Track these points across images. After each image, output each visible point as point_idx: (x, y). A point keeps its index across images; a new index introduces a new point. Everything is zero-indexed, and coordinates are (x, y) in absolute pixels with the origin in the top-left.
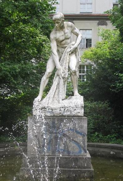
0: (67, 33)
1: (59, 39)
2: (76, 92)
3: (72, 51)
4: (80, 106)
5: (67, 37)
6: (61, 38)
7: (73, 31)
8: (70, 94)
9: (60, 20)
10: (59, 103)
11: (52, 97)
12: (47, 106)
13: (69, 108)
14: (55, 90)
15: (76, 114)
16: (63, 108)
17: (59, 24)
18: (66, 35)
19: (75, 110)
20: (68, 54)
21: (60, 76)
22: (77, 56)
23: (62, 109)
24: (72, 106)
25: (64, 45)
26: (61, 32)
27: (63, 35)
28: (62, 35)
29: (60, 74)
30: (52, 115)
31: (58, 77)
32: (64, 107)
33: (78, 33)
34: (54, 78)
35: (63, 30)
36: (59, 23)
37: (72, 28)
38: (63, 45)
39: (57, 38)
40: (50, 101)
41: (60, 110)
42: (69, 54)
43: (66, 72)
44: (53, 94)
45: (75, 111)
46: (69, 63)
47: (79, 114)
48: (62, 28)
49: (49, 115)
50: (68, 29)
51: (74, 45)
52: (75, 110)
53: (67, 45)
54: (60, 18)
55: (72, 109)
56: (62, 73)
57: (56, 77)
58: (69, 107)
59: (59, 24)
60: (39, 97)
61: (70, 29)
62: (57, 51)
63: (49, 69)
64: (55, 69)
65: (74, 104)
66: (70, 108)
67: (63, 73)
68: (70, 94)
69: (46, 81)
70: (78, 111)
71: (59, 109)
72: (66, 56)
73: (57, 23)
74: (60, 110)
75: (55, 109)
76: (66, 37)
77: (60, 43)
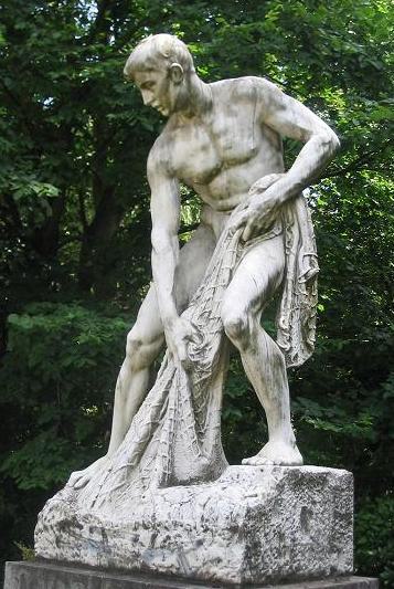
0: (225, 132)
1: (188, 170)
3: (251, 221)
4: (222, 523)
5: (229, 154)
6: (200, 164)
7: (271, 121)
8: (242, 435)
9: (150, 70)
12: (83, 512)
13: (172, 534)
15: (204, 570)
16: (146, 528)
17: (157, 88)
18: (222, 142)
19: (200, 543)
22: (293, 250)
23: (145, 535)
24: (186, 521)
25: (229, 195)
26: (194, 130)
27: (204, 148)
28: (200, 144)
30: (104, 561)
32: (153, 526)
33: (301, 124)
35: (201, 123)
36: (153, 83)
37: (259, 106)
38: (221, 198)
39: (175, 164)
41: (135, 540)
42: (241, 241)
43: (208, 338)
45: (201, 552)
47: (219, 572)
49: (93, 562)
50: (230, 113)
52: (200, 543)
55: (185, 538)
58: (175, 524)
59: (157, 88)
61: (246, 112)
65: (199, 511)
66: (180, 530)
67: (188, 339)
70: (215, 550)
71: (130, 535)
74: (135, 540)
75: (116, 534)
76: (222, 154)
77: (196, 191)
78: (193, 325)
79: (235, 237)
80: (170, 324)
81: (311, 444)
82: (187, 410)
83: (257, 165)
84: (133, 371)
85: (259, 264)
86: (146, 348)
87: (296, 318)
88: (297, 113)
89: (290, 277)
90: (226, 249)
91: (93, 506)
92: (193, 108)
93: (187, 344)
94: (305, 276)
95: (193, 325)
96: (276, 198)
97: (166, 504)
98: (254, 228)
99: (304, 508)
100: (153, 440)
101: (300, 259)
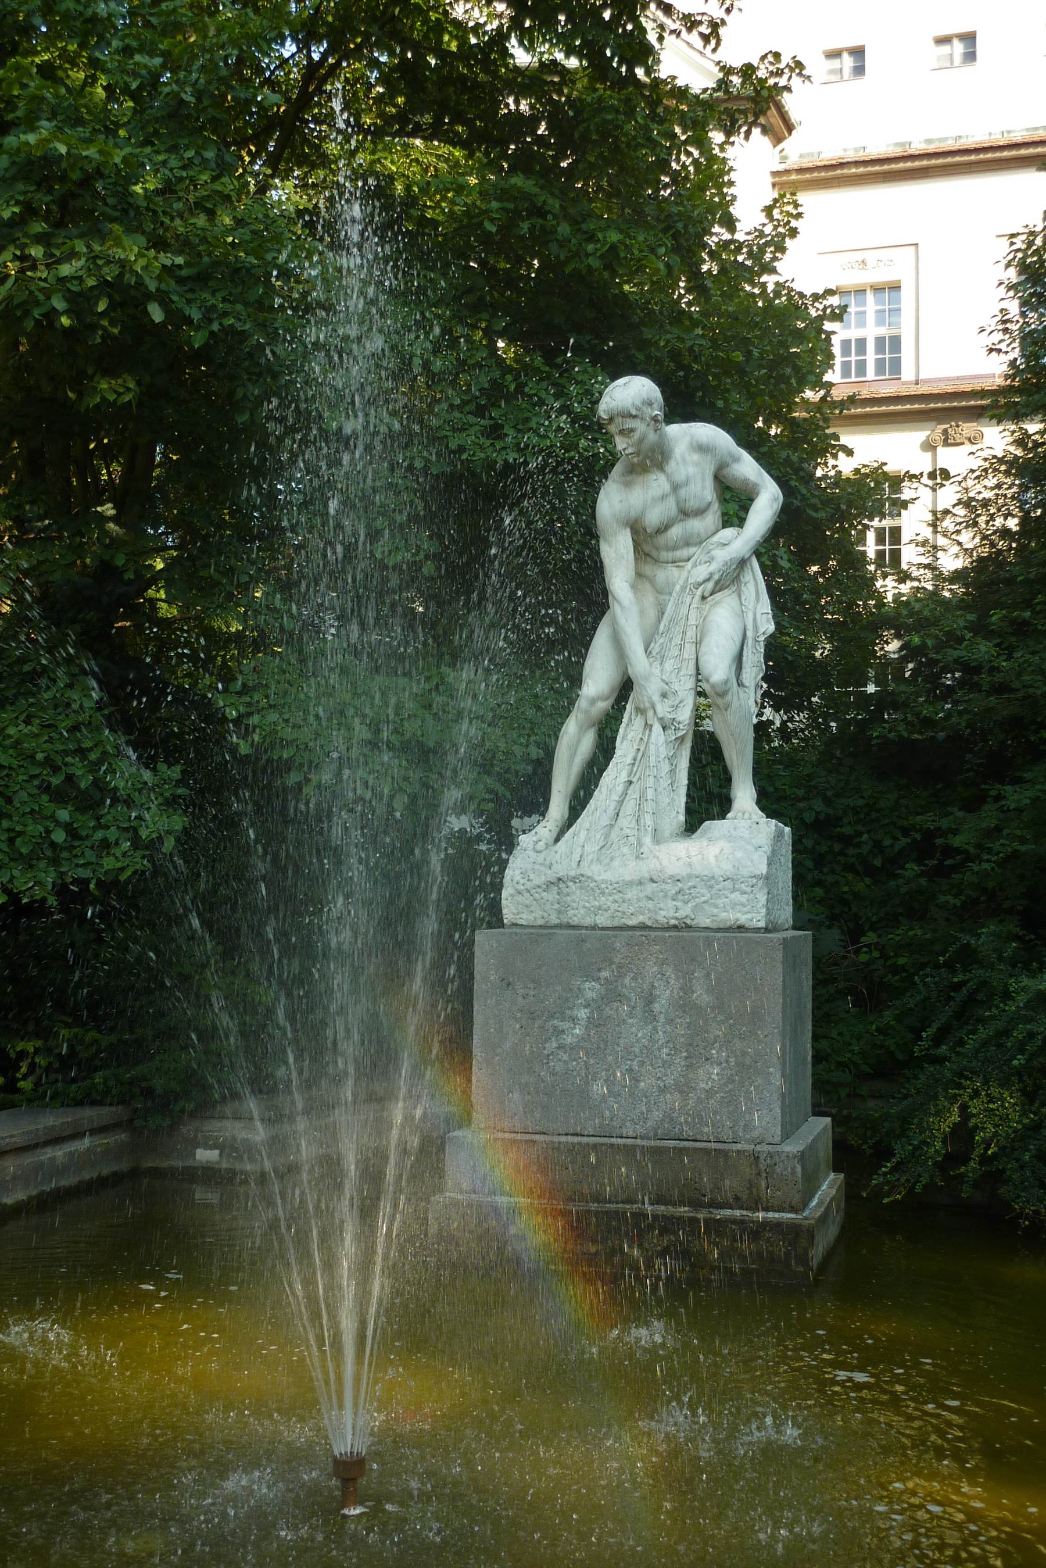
2: (744, 794)
3: (716, 577)
5: (693, 504)
7: (725, 471)
8: (707, 801)
9: (635, 417)
10: (637, 857)
14: (620, 789)
18: (683, 492)
20: (697, 598)
21: (650, 713)
27: (664, 497)
29: (647, 705)
31: (638, 722)
36: (632, 430)
40: (592, 848)
42: (703, 598)
44: (611, 811)
46: (698, 643)
48: (654, 459)
53: (692, 550)
56: (656, 698)
57: (630, 719)
60: (546, 828)
62: (758, 802)
63: (597, 679)
64: (625, 688)
67: (664, 695)
68: (707, 801)
69: (579, 742)
72: (684, 610)
73: (622, 432)
79: (699, 592)
82: (666, 767)
84: (582, 730)
86: (603, 705)
89: (750, 634)
92: (654, 459)
98: (717, 583)
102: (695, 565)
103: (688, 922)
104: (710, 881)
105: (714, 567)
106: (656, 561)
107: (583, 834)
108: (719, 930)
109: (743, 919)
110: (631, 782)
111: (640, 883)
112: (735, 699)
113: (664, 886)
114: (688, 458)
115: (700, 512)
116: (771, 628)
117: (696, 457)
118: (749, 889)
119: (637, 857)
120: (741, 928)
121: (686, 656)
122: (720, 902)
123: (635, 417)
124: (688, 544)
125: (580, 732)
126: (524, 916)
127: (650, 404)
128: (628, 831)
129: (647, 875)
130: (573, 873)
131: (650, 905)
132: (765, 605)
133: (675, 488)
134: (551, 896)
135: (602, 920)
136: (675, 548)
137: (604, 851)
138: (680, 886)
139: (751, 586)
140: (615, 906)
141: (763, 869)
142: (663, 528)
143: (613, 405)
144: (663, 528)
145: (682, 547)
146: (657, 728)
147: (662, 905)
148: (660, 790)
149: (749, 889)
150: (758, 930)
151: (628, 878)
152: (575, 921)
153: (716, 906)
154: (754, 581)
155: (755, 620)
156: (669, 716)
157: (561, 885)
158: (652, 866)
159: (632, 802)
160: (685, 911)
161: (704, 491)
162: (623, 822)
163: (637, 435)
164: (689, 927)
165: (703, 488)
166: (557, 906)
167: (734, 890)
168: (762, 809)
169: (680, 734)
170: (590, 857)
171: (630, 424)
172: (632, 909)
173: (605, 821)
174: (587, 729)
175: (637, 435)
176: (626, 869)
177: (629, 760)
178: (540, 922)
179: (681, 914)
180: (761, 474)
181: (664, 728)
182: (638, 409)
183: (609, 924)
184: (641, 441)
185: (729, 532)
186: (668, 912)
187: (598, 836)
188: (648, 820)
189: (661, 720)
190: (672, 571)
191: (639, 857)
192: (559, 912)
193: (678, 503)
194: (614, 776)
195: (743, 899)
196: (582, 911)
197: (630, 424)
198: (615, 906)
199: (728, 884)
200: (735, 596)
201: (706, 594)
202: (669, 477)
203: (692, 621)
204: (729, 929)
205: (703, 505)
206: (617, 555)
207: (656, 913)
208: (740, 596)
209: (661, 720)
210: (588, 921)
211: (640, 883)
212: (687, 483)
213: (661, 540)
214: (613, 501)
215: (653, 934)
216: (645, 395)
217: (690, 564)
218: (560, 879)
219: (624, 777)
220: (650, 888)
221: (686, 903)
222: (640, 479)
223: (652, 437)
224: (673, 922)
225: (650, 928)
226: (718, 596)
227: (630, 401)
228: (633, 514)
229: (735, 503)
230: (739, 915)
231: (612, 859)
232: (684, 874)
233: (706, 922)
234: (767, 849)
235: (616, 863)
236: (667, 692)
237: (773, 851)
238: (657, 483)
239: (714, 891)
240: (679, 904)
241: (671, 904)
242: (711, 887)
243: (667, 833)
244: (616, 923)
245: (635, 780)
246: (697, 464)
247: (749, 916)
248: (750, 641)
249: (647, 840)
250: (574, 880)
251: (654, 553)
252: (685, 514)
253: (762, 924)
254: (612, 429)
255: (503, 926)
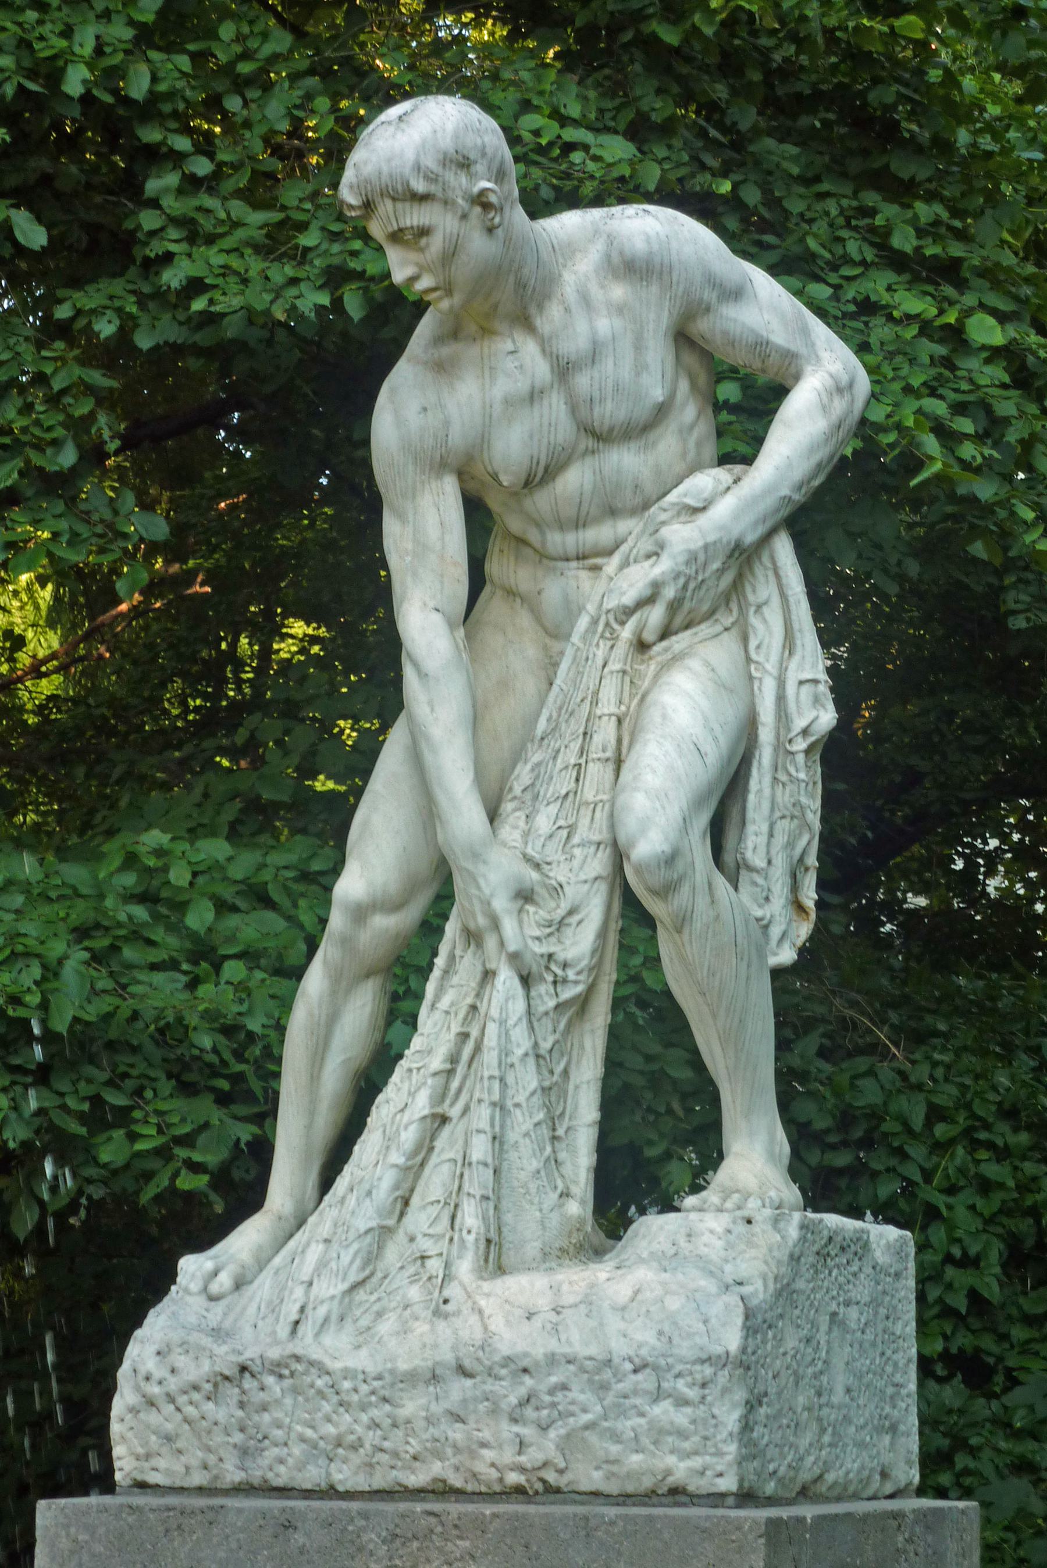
0: (594, 354)
3: (670, 592)
5: (609, 412)
6: (512, 448)
7: (702, 326)
8: (647, 1152)
9: (423, 198)
10: (437, 1313)
11: (362, 1224)
18: (583, 382)
20: (622, 648)
21: (491, 943)
27: (534, 396)
33: (779, 337)
34: (430, 987)
36: (424, 232)
40: (330, 1288)
42: (642, 646)
48: (509, 299)
51: (703, 520)
53: (624, 526)
54: (418, 167)
56: (501, 904)
57: (452, 959)
63: (372, 864)
67: (525, 896)
68: (647, 1152)
69: (333, 1018)
72: (590, 681)
73: (396, 237)
78: (527, 859)
79: (626, 633)
80: (476, 856)
81: (822, 1182)
82: (527, 1080)
83: (668, 445)
84: (341, 984)
85: (685, 710)
86: (386, 925)
87: (780, 840)
88: (766, 307)
89: (766, 735)
90: (595, 664)
91: (294, 1331)
92: (509, 299)
93: (520, 911)
94: (805, 732)
95: (527, 859)
96: (735, 534)
97: (519, 1310)
98: (674, 607)
99: (834, 1314)
100: (434, 1159)
101: (791, 690)
102: (625, 564)
103: (551, 1477)
104: (599, 1372)
105: (663, 567)
106: (543, 556)
107: (315, 1252)
108: (625, 1498)
109: (681, 1469)
110: (444, 1119)
111: (434, 1378)
112: (702, 902)
113: (491, 1386)
114: (596, 293)
115: (640, 429)
116: (827, 718)
117: (619, 292)
118: (692, 1394)
119: (437, 1313)
120: (677, 1493)
121: (589, 794)
122: (627, 1425)
123: (423, 198)
124: (612, 512)
125: (333, 993)
126: (162, 1463)
127: (464, 164)
128: (426, 1245)
129: (449, 1357)
130: (274, 1353)
131: (457, 1433)
132: (811, 662)
133: (564, 370)
134: (222, 1412)
135: (345, 1475)
136: (579, 523)
137: (361, 1295)
138: (527, 1383)
139: (774, 615)
140: (371, 1438)
141: (732, 1340)
142: (540, 476)
143: (368, 170)
144: (540, 476)
145: (597, 520)
146: (506, 979)
147: (486, 1435)
148: (512, 1136)
149: (692, 1394)
150: (717, 1499)
151: (403, 1366)
152: (282, 1476)
153: (616, 1437)
154: (784, 548)
155: (781, 699)
156: (539, 949)
157: (248, 1383)
158: (465, 1334)
159: (446, 1168)
160: (544, 1448)
161: (650, 373)
162: (418, 1219)
163: (436, 244)
164: (552, 1491)
165: (640, 368)
166: (238, 1438)
167: (658, 1395)
168: (166, 1291)
169: (568, 993)
170: (322, 1311)
171: (414, 217)
172: (415, 1446)
173: (366, 1218)
174: (368, 976)
175: (436, 244)
176: (405, 1339)
177: (437, 1062)
178: (198, 1479)
179: (532, 1457)
180: (805, 331)
181: (526, 981)
182: (431, 178)
183: (361, 1482)
184: (450, 255)
185: (723, 475)
186: (500, 1452)
187: (346, 1258)
188: (470, 1217)
189: (515, 958)
190: (578, 577)
191: (441, 1309)
192: (244, 1452)
193: (573, 409)
194: (402, 1103)
195: (681, 1418)
196: (297, 1450)
197: (414, 217)
198: (371, 1438)
199: (645, 1380)
200: (730, 642)
201: (649, 636)
202: (545, 346)
203: (608, 705)
204: (648, 1497)
205: (642, 413)
206: (422, 543)
207: (473, 1455)
208: (745, 639)
209: (515, 958)
210: (312, 1476)
211: (434, 1378)
212: (594, 354)
213: (542, 501)
214: (408, 413)
215: (454, 1509)
216: (447, 143)
217: (616, 560)
218: (243, 1369)
219: (422, 1105)
220: (458, 1389)
221: (544, 1428)
222: (472, 351)
223: (479, 246)
224: (513, 1478)
225: (458, 1494)
226: (679, 642)
227: (410, 156)
228: (457, 438)
229: (743, 403)
230: (671, 1460)
231: (379, 1314)
232: (539, 1352)
233: (592, 1478)
234: (758, 1291)
235: (386, 1327)
236: (538, 883)
237: (785, 1292)
238: (520, 361)
239: (610, 1399)
240: (527, 1431)
241: (508, 1430)
242: (605, 1387)
243: (532, 1249)
244: (378, 1481)
245: (454, 1112)
246: (620, 310)
247: (696, 1462)
248: (765, 755)
249: (465, 1267)
250: (277, 1368)
251: (533, 536)
252: (600, 436)
253: (728, 1484)
254: (377, 230)
255: (105, 1482)
